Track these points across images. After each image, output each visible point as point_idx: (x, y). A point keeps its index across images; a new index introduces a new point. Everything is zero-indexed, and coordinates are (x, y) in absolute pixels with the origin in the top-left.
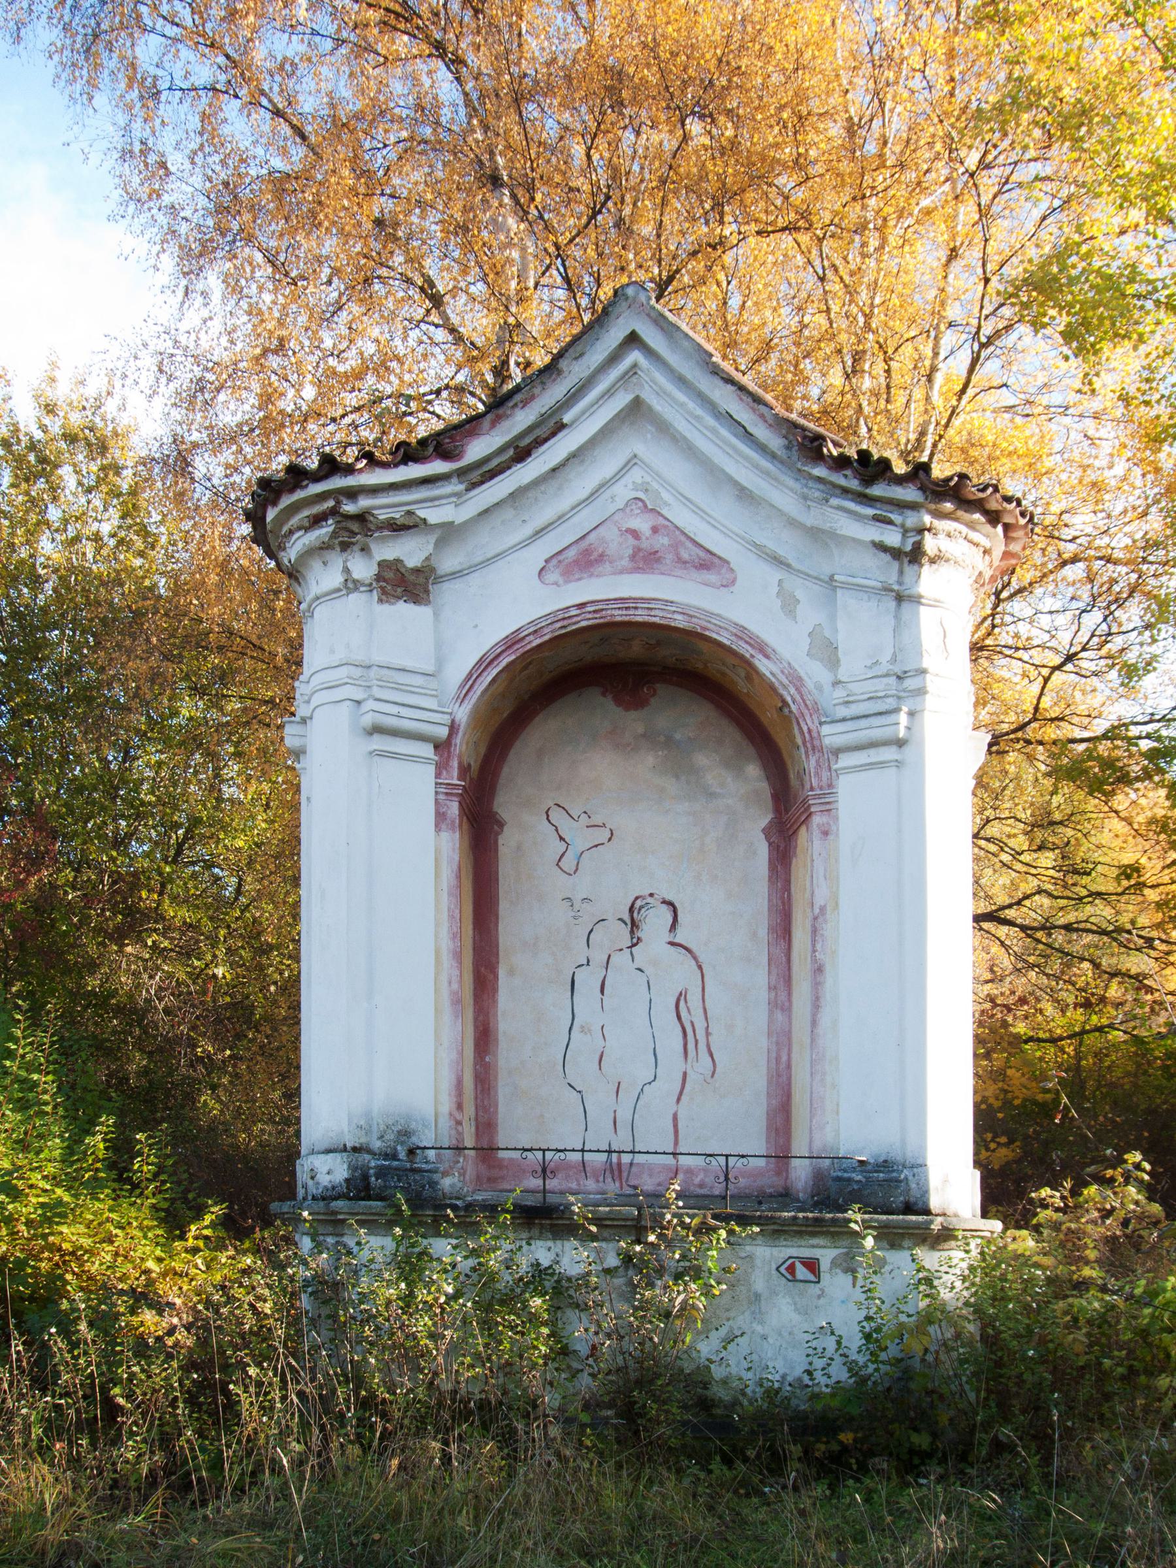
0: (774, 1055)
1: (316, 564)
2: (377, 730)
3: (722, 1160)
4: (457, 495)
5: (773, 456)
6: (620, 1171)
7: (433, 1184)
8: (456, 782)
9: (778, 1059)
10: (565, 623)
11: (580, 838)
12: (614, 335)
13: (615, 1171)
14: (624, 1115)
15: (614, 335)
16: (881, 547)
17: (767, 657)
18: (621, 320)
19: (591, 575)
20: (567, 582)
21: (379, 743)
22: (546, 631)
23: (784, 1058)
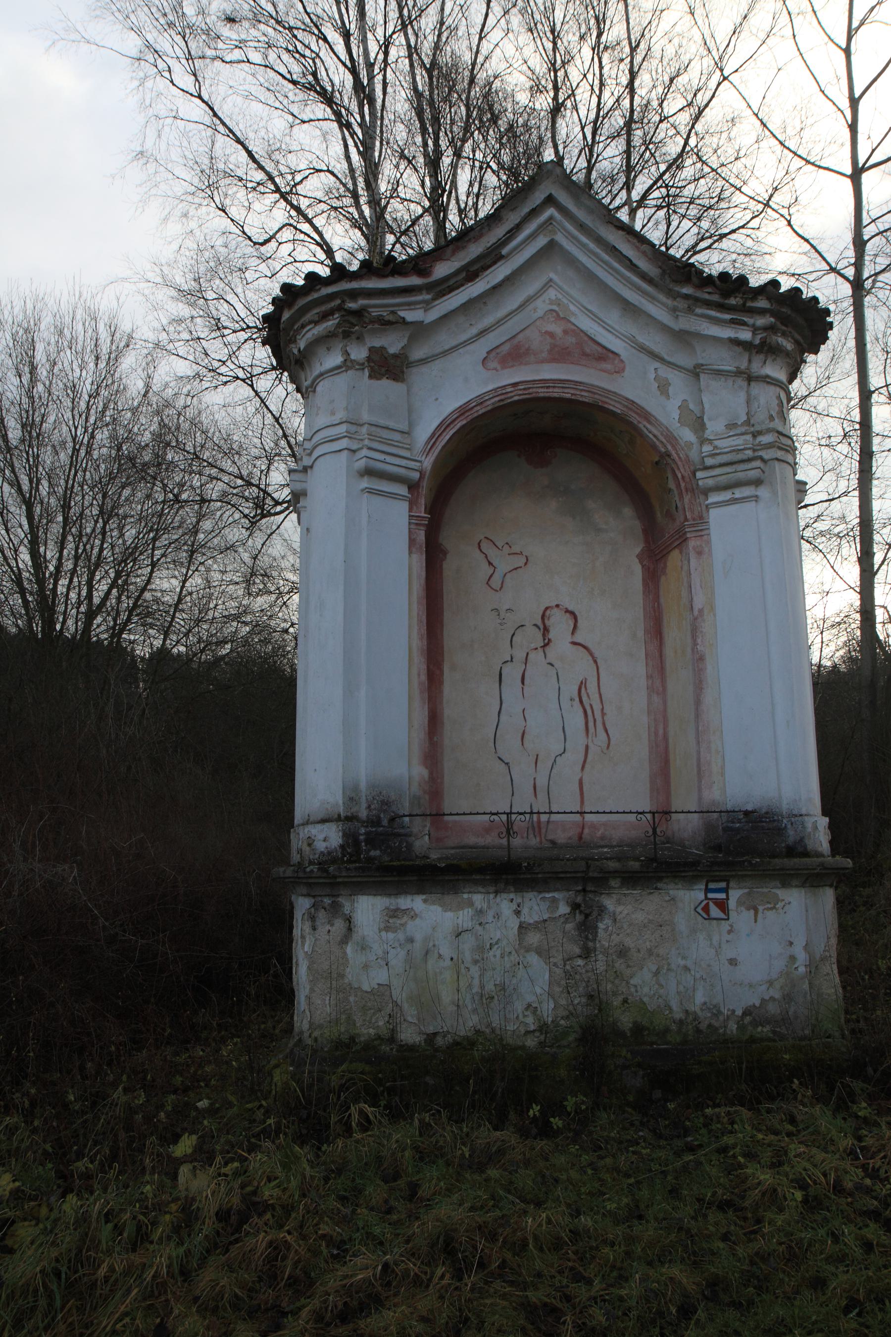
0: (653, 729)
1: (321, 351)
2: (369, 472)
3: (649, 816)
4: (427, 302)
5: (649, 280)
6: (540, 828)
7: (409, 846)
8: (423, 515)
9: (656, 734)
10: (502, 397)
11: (503, 564)
12: (538, 197)
13: (536, 828)
14: (542, 782)
15: (538, 197)
16: (736, 342)
17: (649, 422)
18: (542, 187)
19: (521, 364)
20: (504, 368)
21: (365, 483)
22: (489, 403)
23: (661, 732)
